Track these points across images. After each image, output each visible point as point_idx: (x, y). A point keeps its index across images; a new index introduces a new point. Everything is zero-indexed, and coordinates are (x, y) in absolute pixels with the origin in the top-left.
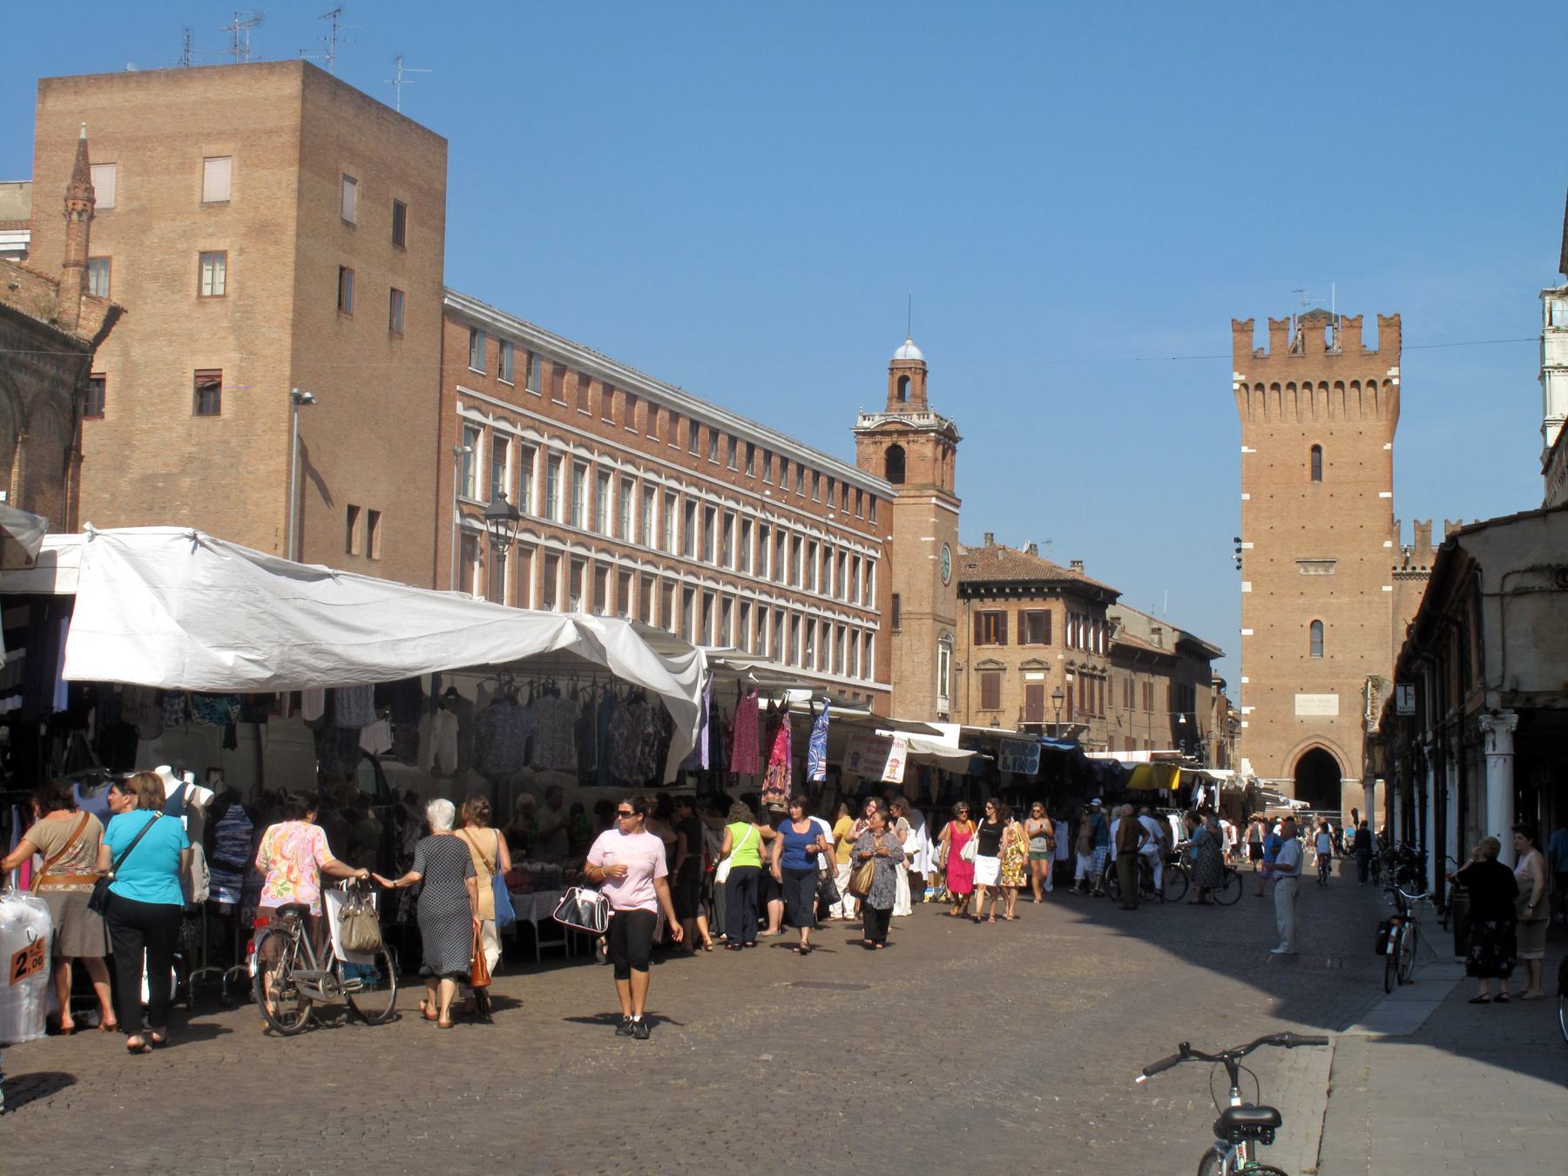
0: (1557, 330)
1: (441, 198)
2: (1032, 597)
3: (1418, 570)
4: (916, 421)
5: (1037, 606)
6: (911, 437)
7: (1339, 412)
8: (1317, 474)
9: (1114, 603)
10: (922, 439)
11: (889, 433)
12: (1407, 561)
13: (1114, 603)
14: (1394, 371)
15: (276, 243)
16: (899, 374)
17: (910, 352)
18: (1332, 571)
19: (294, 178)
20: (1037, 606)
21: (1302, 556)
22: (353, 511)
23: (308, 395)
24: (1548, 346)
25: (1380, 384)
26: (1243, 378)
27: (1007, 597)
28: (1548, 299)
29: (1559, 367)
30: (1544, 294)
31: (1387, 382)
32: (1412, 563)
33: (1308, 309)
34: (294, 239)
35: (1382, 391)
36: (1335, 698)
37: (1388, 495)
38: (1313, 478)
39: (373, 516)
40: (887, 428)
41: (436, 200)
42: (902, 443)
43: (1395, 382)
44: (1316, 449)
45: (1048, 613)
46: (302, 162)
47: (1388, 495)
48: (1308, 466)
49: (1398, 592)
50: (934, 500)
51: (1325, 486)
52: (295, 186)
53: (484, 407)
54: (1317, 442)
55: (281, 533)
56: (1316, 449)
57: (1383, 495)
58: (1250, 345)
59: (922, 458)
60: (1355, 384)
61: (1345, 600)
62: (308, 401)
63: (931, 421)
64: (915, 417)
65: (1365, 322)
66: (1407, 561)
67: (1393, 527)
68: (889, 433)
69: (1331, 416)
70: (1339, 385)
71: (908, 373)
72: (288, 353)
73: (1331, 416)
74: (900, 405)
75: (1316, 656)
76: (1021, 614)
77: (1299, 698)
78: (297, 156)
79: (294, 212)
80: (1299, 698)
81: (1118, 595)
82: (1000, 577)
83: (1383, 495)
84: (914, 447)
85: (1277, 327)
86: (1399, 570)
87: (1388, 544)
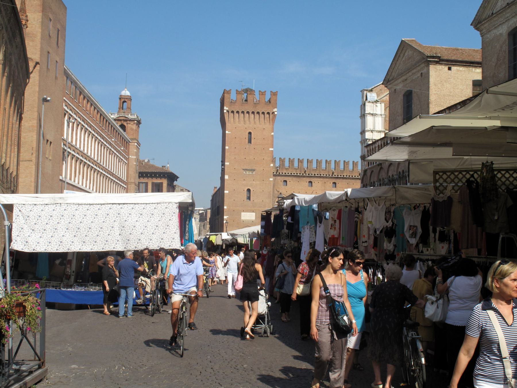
0: (369, 102)
1: (65, 27)
2: (157, 177)
3: (281, 174)
4: (130, 117)
5: (158, 181)
6: (128, 122)
7: (257, 122)
8: (250, 141)
9: (177, 181)
10: (132, 123)
11: (120, 120)
12: (277, 171)
13: (177, 181)
14: (275, 110)
15: (33, 41)
16: (123, 100)
17: (126, 93)
18: (254, 173)
19: (40, 17)
20: (158, 181)
21: (245, 167)
22: (48, 141)
23: (49, 99)
24: (366, 107)
25: (271, 114)
26: (227, 109)
27: (148, 177)
28: (365, 92)
29: (369, 114)
30: (362, 91)
31: (273, 113)
32: (335, 174)
33: (245, 88)
34: (40, 40)
35: (271, 115)
36: (254, 214)
37: (272, 149)
38: (249, 142)
39: (51, 143)
40: (120, 118)
41: (64, 28)
42: (125, 124)
43: (276, 113)
44: (250, 133)
45: (162, 183)
46: (43, 11)
47: (272, 149)
48: (247, 138)
49: (274, 180)
50: (136, 144)
51: (252, 145)
52: (40, 20)
53: (68, 106)
54: (250, 131)
55: (35, 149)
56: (250, 133)
57: (271, 149)
58: (230, 98)
59: (132, 129)
60: (263, 113)
61: (258, 182)
62: (48, 101)
63: (135, 117)
64: (130, 115)
65: (232, 92)
66: (277, 171)
67: (273, 161)
68: (120, 120)
69: (255, 123)
70: (258, 113)
71: (126, 100)
72: (38, 82)
73: (255, 123)
74: (123, 111)
75: (248, 200)
76: (153, 183)
77: (243, 214)
78: (41, 9)
79: (40, 30)
80: (243, 214)
81: (178, 178)
82: (147, 171)
83: (271, 149)
84: (129, 125)
85: (238, 92)
86: (275, 174)
87: (272, 165)
